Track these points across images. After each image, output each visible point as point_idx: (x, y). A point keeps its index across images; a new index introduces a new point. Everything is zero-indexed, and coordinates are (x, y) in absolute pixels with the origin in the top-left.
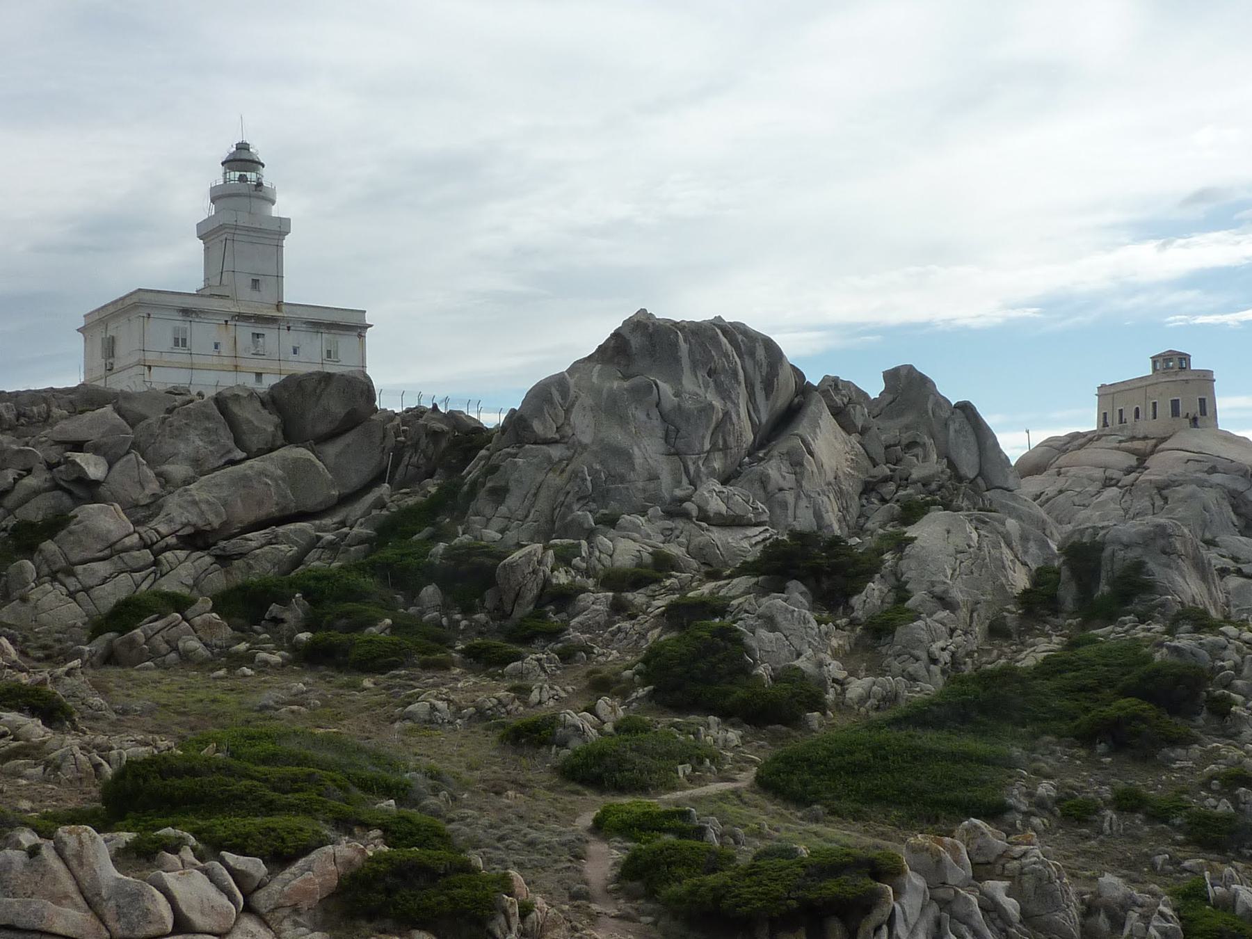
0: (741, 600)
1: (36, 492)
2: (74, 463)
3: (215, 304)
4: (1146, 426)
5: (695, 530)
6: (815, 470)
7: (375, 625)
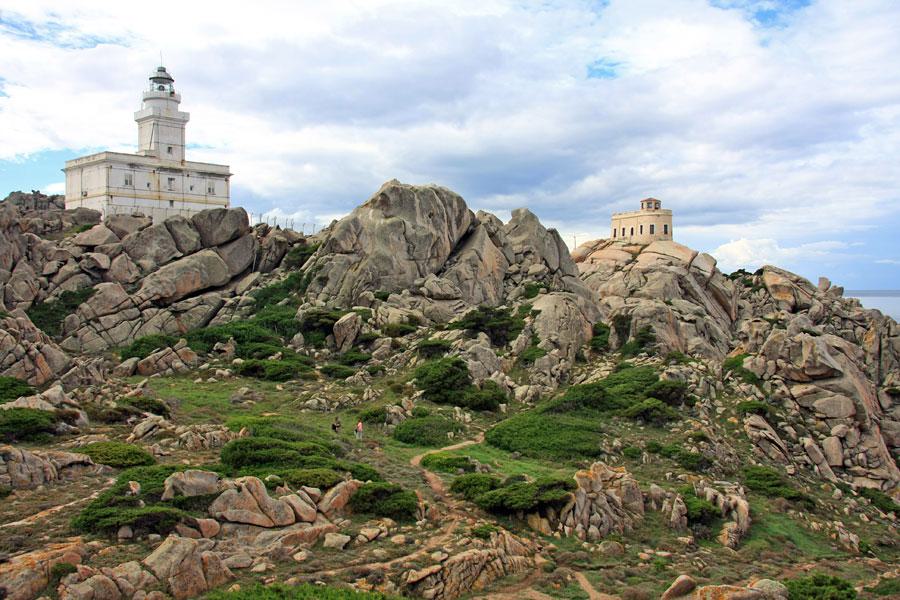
0: (456, 342)
1: (71, 275)
4: (637, 238)
5: (427, 303)
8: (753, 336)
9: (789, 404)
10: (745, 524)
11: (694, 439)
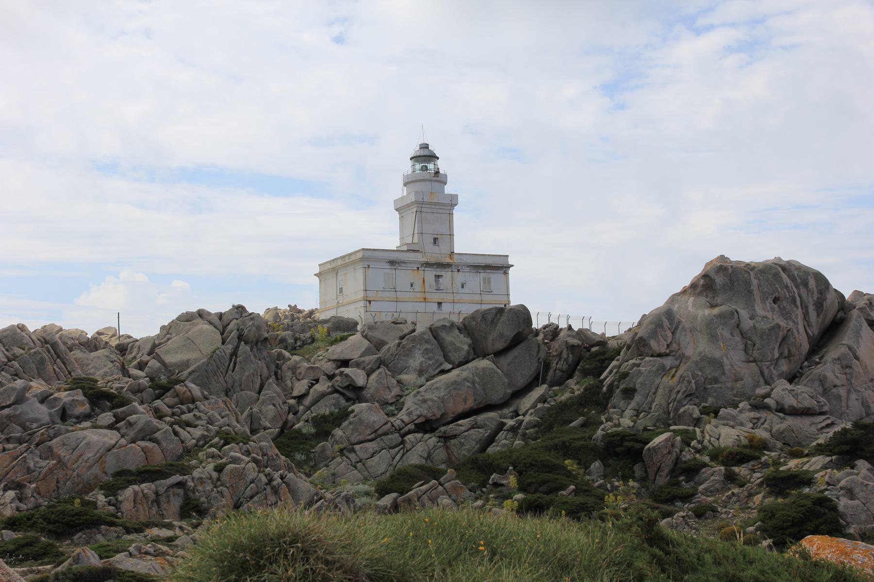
1: (323, 395)
2: (347, 376)
3: (411, 256)
5: (776, 419)
6: (861, 371)
7: (564, 489)
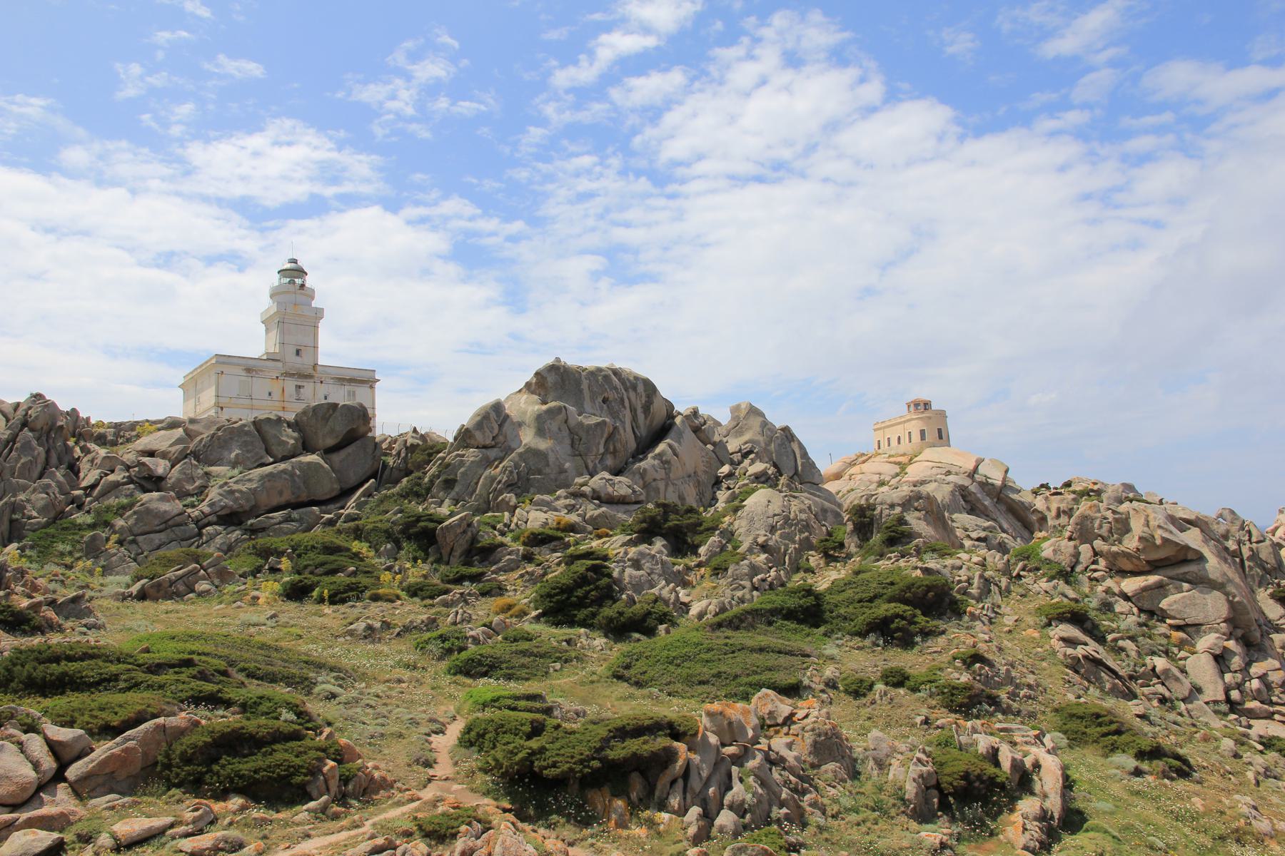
8: (1054, 513)
9: (1121, 606)
10: (1054, 804)
11: (964, 662)
